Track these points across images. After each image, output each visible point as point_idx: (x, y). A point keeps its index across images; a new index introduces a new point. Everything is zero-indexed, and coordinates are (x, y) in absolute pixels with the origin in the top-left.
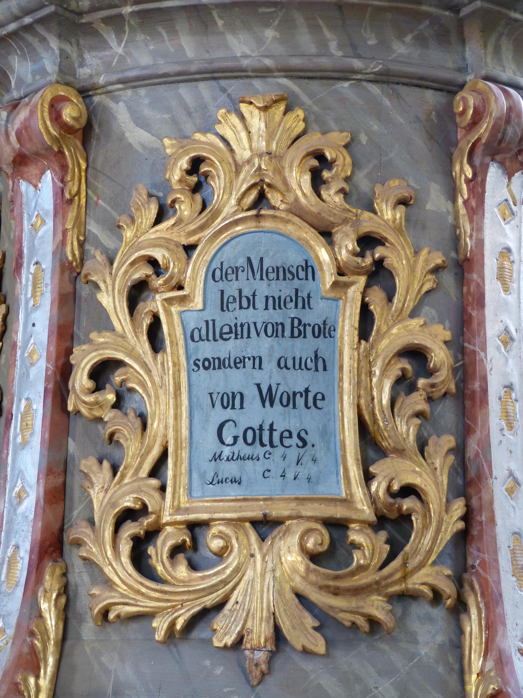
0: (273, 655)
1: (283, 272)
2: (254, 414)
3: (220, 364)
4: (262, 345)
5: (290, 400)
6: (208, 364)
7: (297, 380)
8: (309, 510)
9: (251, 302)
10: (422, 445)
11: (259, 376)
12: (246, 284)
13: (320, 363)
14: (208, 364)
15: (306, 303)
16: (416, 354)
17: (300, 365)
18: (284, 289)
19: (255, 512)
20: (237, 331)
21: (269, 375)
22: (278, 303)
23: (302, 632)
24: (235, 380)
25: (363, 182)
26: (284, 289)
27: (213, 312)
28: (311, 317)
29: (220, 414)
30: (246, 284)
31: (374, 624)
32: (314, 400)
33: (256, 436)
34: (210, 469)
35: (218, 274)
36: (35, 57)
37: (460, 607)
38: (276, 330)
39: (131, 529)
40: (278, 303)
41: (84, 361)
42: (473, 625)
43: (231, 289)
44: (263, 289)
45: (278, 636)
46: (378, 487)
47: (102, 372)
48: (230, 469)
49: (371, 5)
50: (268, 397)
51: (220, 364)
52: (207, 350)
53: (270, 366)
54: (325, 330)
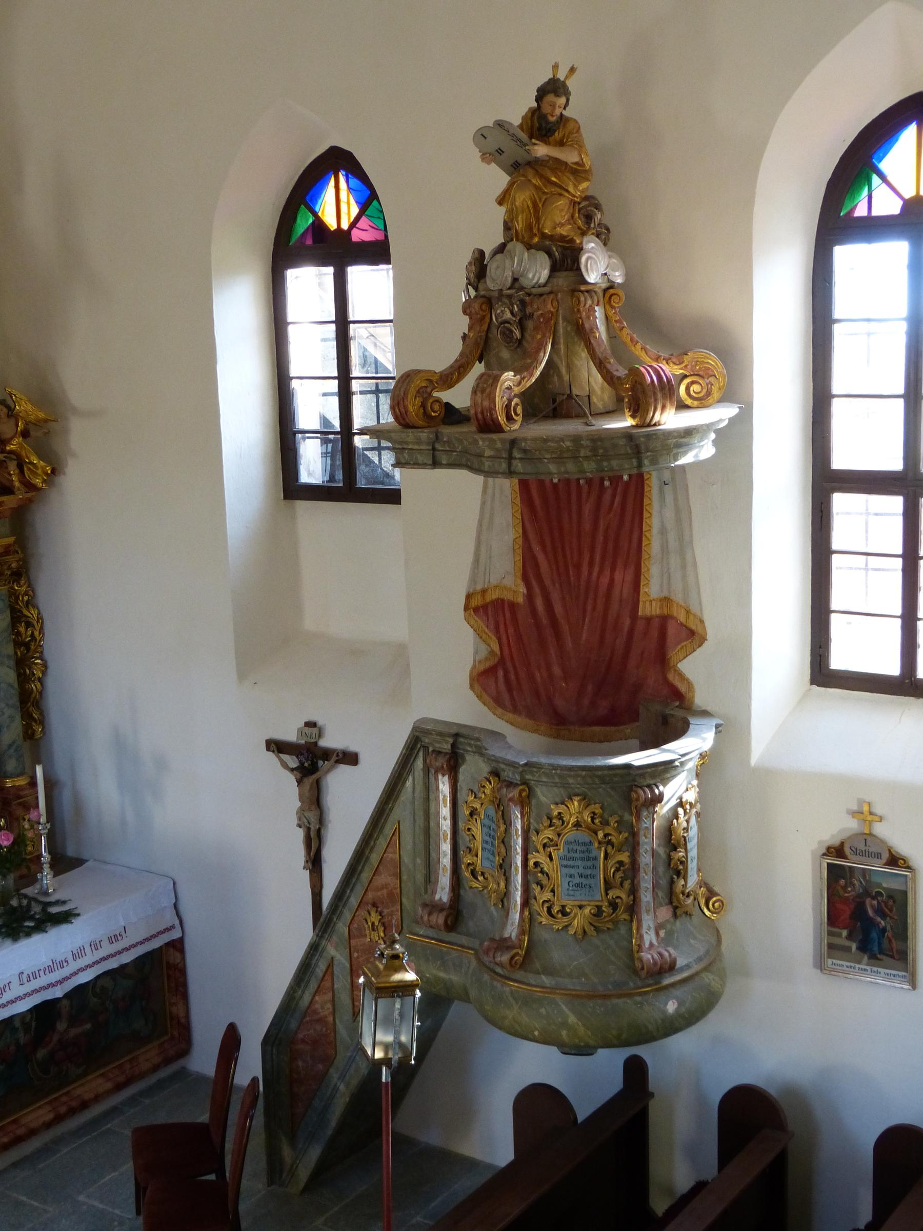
0: (583, 937)
1: (584, 844)
2: (577, 880)
3: (568, 867)
4: (579, 863)
5: (586, 877)
6: (565, 866)
7: (589, 872)
8: (592, 903)
9: (576, 851)
10: (621, 884)
11: (578, 871)
12: (575, 847)
13: (594, 867)
14: (565, 866)
15: (591, 852)
16: (621, 863)
17: (589, 868)
18: (584, 848)
19: (578, 903)
20: (572, 859)
21: (581, 870)
22: (583, 852)
23: (590, 930)
24: (572, 871)
25: (606, 816)
26: (584, 848)
27: (566, 852)
28: (592, 855)
29: (568, 879)
30: (575, 847)
31: (608, 929)
32: (592, 876)
33: (578, 885)
34: (566, 892)
35: (567, 843)
36: (441, 899)
37: (632, 921)
38: (583, 859)
39: (546, 905)
40: (583, 852)
41: (531, 863)
42: (634, 925)
43: (571, 847)
44: (579, 848)
45: (585, 932)
46: (610, 897)
47: (536, 864)
48: (572, 893)
49: (708, 427)
50: (581, 876)
51: (568, 867)
52: (565, 863)
53: (581, 868)
54: (596, 859)
